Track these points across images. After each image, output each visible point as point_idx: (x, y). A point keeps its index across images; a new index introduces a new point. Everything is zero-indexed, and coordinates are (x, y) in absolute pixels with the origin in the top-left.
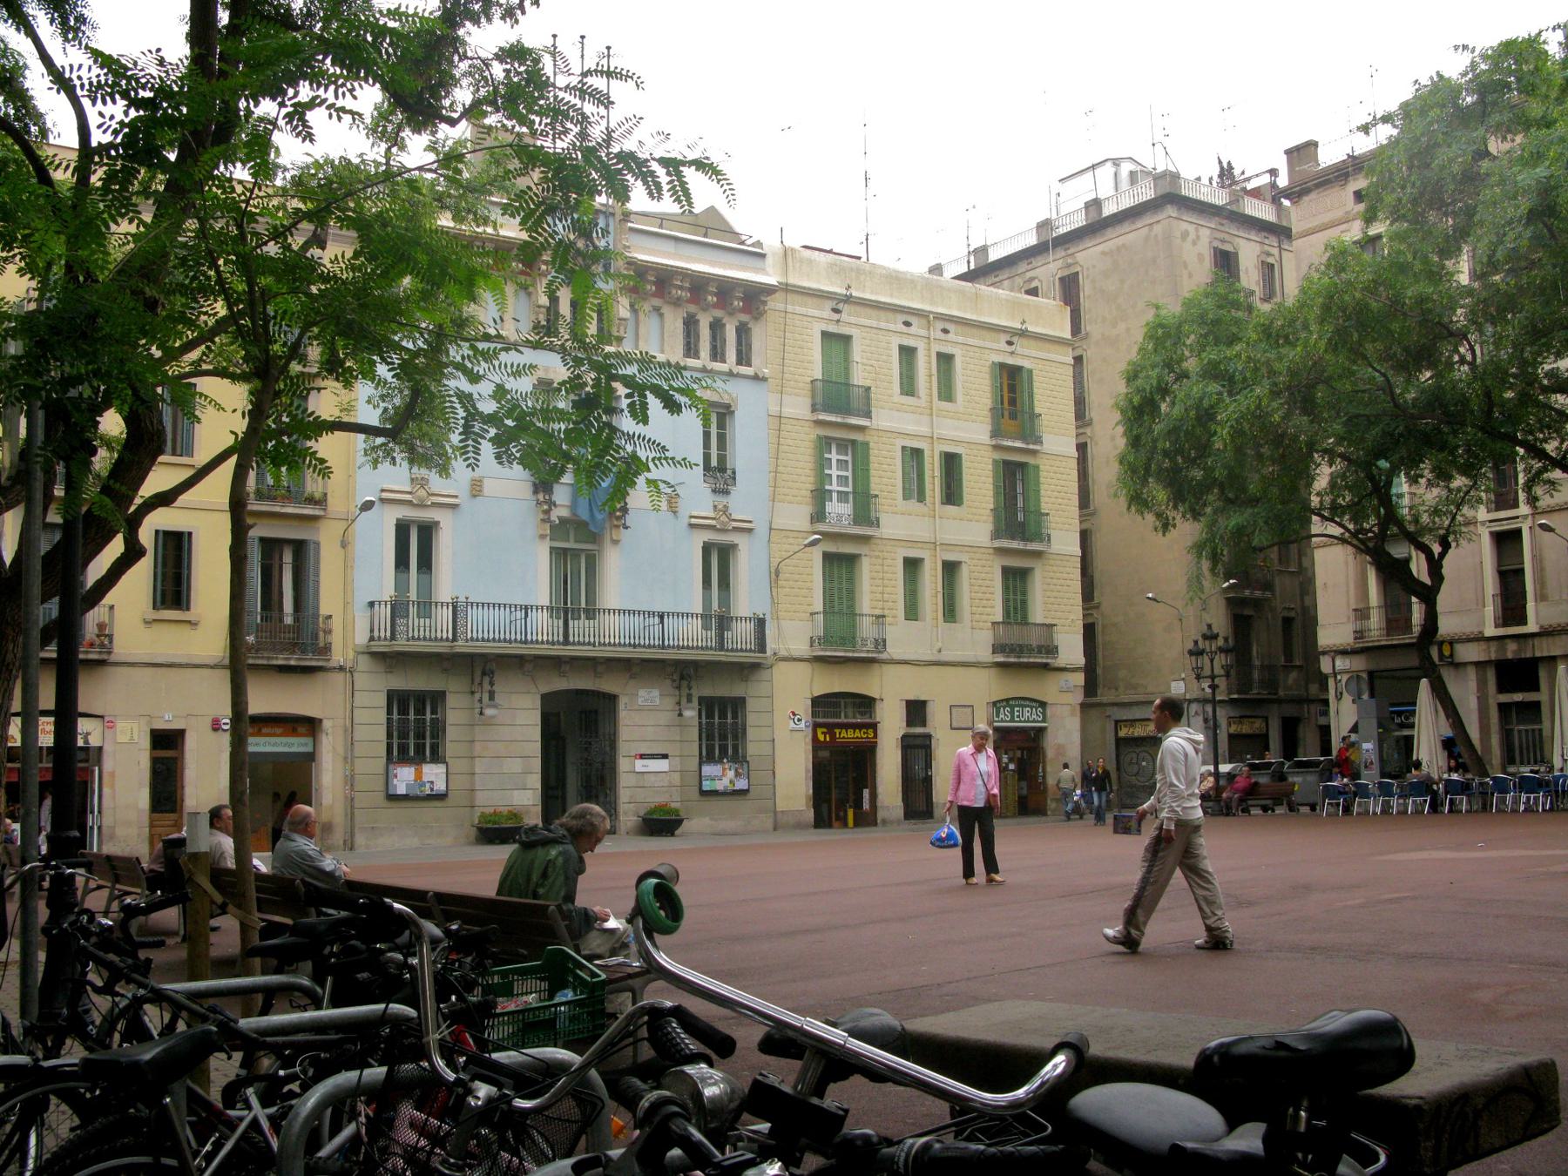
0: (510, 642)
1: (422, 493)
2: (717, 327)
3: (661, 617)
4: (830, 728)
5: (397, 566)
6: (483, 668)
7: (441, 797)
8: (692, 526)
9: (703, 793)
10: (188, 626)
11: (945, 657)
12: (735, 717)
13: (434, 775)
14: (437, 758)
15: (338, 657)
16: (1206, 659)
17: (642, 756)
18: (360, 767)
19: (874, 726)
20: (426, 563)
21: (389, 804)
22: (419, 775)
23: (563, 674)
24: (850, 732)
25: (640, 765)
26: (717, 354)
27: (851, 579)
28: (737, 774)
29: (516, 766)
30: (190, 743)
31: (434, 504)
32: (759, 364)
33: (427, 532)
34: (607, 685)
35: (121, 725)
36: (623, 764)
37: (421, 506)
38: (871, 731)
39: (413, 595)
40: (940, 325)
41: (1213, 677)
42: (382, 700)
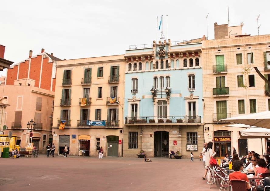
1: (191, 97)
2: (135, 64)
4: (218, 138)
8: (128, 101)
12: (130, 136)
16: (30, 126)
19: (230, 137)
20: (136, 111)
23: (158, 128)
24: (223, 139)
26: (191, 64)
27: (226, 106)
31: (136, 101)
32: (143, 70)
34: (167, 130)
37: (134, 101)
38: (229, 139)
40: (248, 47)
42: (128, 133)
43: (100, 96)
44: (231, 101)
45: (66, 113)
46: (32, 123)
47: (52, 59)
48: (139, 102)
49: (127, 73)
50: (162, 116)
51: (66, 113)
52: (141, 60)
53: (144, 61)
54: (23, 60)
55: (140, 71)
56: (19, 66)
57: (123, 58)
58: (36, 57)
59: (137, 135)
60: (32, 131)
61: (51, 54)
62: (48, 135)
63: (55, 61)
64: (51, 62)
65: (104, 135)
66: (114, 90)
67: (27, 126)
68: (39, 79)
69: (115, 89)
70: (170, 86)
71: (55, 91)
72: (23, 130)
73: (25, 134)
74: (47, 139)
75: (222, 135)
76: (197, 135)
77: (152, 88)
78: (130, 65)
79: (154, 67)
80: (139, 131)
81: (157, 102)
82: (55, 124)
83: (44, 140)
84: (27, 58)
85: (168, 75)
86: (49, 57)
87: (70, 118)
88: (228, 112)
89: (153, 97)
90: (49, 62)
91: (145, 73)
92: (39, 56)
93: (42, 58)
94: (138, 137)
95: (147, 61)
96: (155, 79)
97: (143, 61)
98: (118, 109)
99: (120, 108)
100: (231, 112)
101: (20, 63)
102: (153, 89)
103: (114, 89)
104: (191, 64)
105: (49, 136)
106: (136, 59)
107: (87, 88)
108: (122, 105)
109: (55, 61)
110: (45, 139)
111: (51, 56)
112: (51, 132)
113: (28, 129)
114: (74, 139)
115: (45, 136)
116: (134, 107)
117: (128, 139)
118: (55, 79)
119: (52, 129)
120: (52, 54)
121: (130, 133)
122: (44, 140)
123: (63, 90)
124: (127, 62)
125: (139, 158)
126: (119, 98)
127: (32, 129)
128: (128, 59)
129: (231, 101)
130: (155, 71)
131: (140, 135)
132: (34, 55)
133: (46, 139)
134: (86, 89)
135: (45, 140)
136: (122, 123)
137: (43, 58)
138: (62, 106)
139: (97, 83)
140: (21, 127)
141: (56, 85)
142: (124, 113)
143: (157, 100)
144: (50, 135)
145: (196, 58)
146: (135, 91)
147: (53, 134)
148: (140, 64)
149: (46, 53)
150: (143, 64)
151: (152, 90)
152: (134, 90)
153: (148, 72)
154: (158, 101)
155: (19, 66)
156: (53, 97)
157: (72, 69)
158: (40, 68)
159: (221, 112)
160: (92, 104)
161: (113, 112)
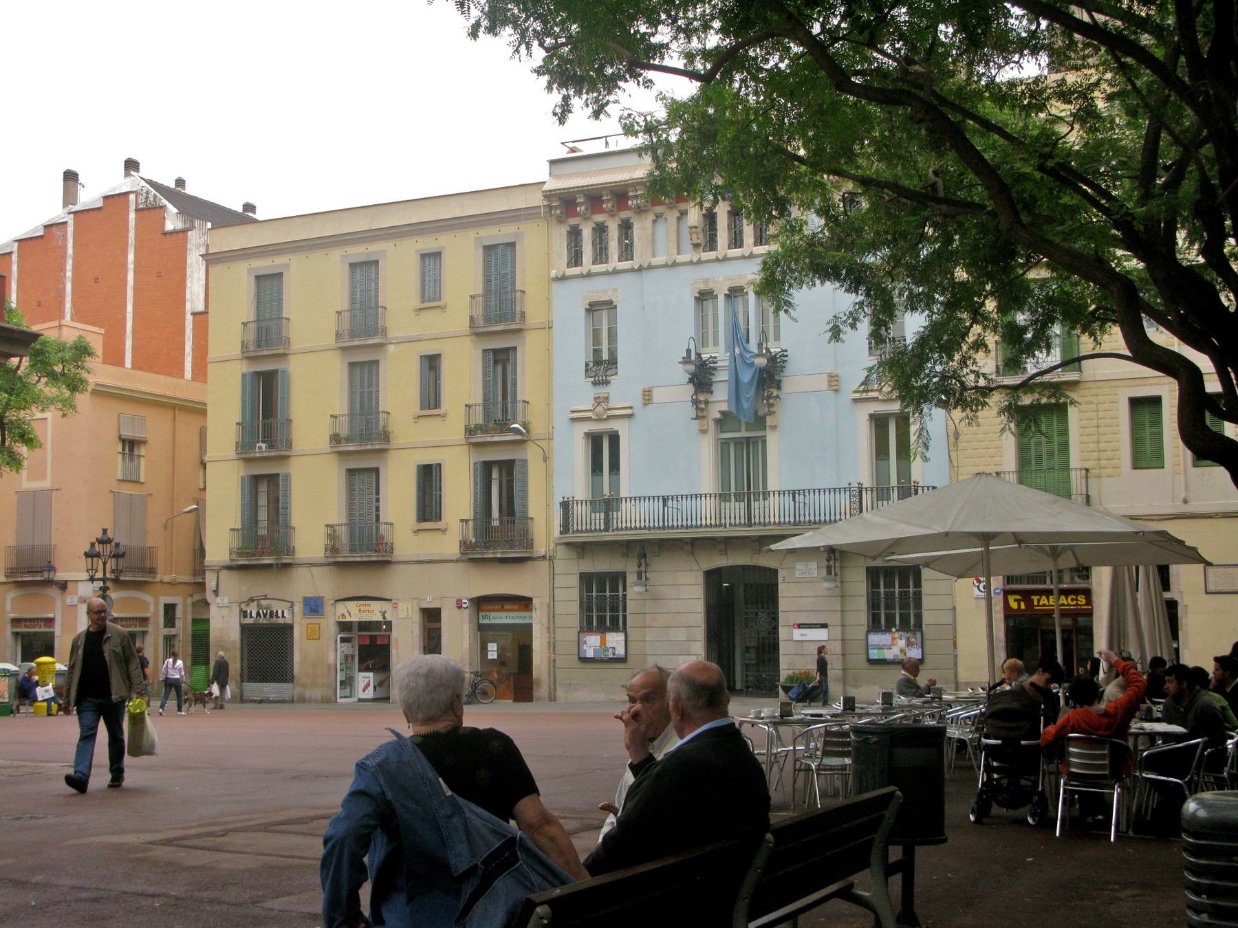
0: (649, 528)
2: (600, 230)
3: (665, 500)
4: (1026, 595)
5: (593, 471)
6: (645, 550)
7: (623, 660)
8: (573, 420)
9: (872, 662)
10: (439, 533)
11: (1195, 507)
12: (589, 598)
13: (615, 641)
14: (614, 627)
15: (541, 548)
17: (800, 626)
18: (560, 635)
20: (615, 466)
21: (583, 665)
22: (603, 642)
25: (797, 634)
26: (601, 255)
28: (909, 644)
29: (681, 635)
30: (444, 616)
33: (614, 439)
35: (401, 605)
36: (783, 633)
37: (600, 420)
39: (894, 481)
41: (104, 580)
42: (575, 581)
43: (431, 398)
44: (1090, 403)
45: (266, 490)
46: (108, 549)
47: (182, 212)
48: (625, 422)
49: (563, 278)
50: (733, 490)
51: (266, 490)
52: (629, 208)
53: (646, 211)
54: (30, 223)
55: (626, 265)
56: (15, 257)
57: (537, 200)
58: (100, 204)
59: (621, 588)
60: (109, 584)
61: (172, 185)
62: (185, 605)
63: (197, 223)
64: (179, 225)
65: (457, 595)
66: (499, 368)
67: (83, 562)
68: (125, 318)
69: (504, 363)
70: (777, 338)
71: (205, 381)
72: (63, 586)
73: (75, 601)
74: (183, 626)
75: (1048, 581)
76: (918, 584)
77: (689, 351)
78: (575, 234)
79: (696, 241)
80: (630, 567)
81: (717, 421)
82: (219, 549)
83: (167, 631)
84: (52, 209)
85: (702, 287)
86: (165, 202)
87: (287, 516)
88: (1075, 460)
89: (696, 393)
90: (169, 226)
91: (655, 272)
92: (115, 201)
93: (132, 207)
94: (625, 596)
95: (659, 209)
96: (704, 297)
97: (640, 211)
98: (525, 462)
99: (532, 455)
100: (1088, 465)
101: (20, 241)
102: (693, 357)
103: (500, 361)
104: (601, 255)
105: (190, 609)
106: (603, 202)
107: (364, 363)
108: (542, 443)
109: (197, 223)
110: (173, 626)
111: (176, 194)
112: (201, 586)
113: (92, 579)
114: (314, 620)
115: (170, 609)
116: (603, 451)
117: (575, 608)
118: (201, 317)
119: (203, 573)
120: (180, 182)
121: (586, 580)
122: (167, 631)
123: (244, 376)
124: (560, 221)
125: (351, 685)
126: (525, 410)
127: (108, 575)
128: (565, 204)
129: (1090, 403)
130: (700, 262)
131: (633, 591)
132: (89, 196)
133: (179, 623)
134: (362, 364)
135: (172, 631)
136: (544, 527)
137: (137, 210)
138: (244, 448)
139: (413, 332)
140: (51, 568)
141: (212, 354)
142: (557, 478)
143: (715, 412)
144: (194, 604)
145: (571, 227)
146: (602, 366)
147: (209, 596)
148: (626, 227)
149: (150, 182)
150: (641, 228)
151: (686, 360)
152: (598, 362)
153: (666, 266)
154: (718, 416)
155: (15, 257)
156: (199, 410)
157: (287, 266)
158: (64, 270)
159: (1039, 464)
160: (396, 441)
161: (501, 479)
